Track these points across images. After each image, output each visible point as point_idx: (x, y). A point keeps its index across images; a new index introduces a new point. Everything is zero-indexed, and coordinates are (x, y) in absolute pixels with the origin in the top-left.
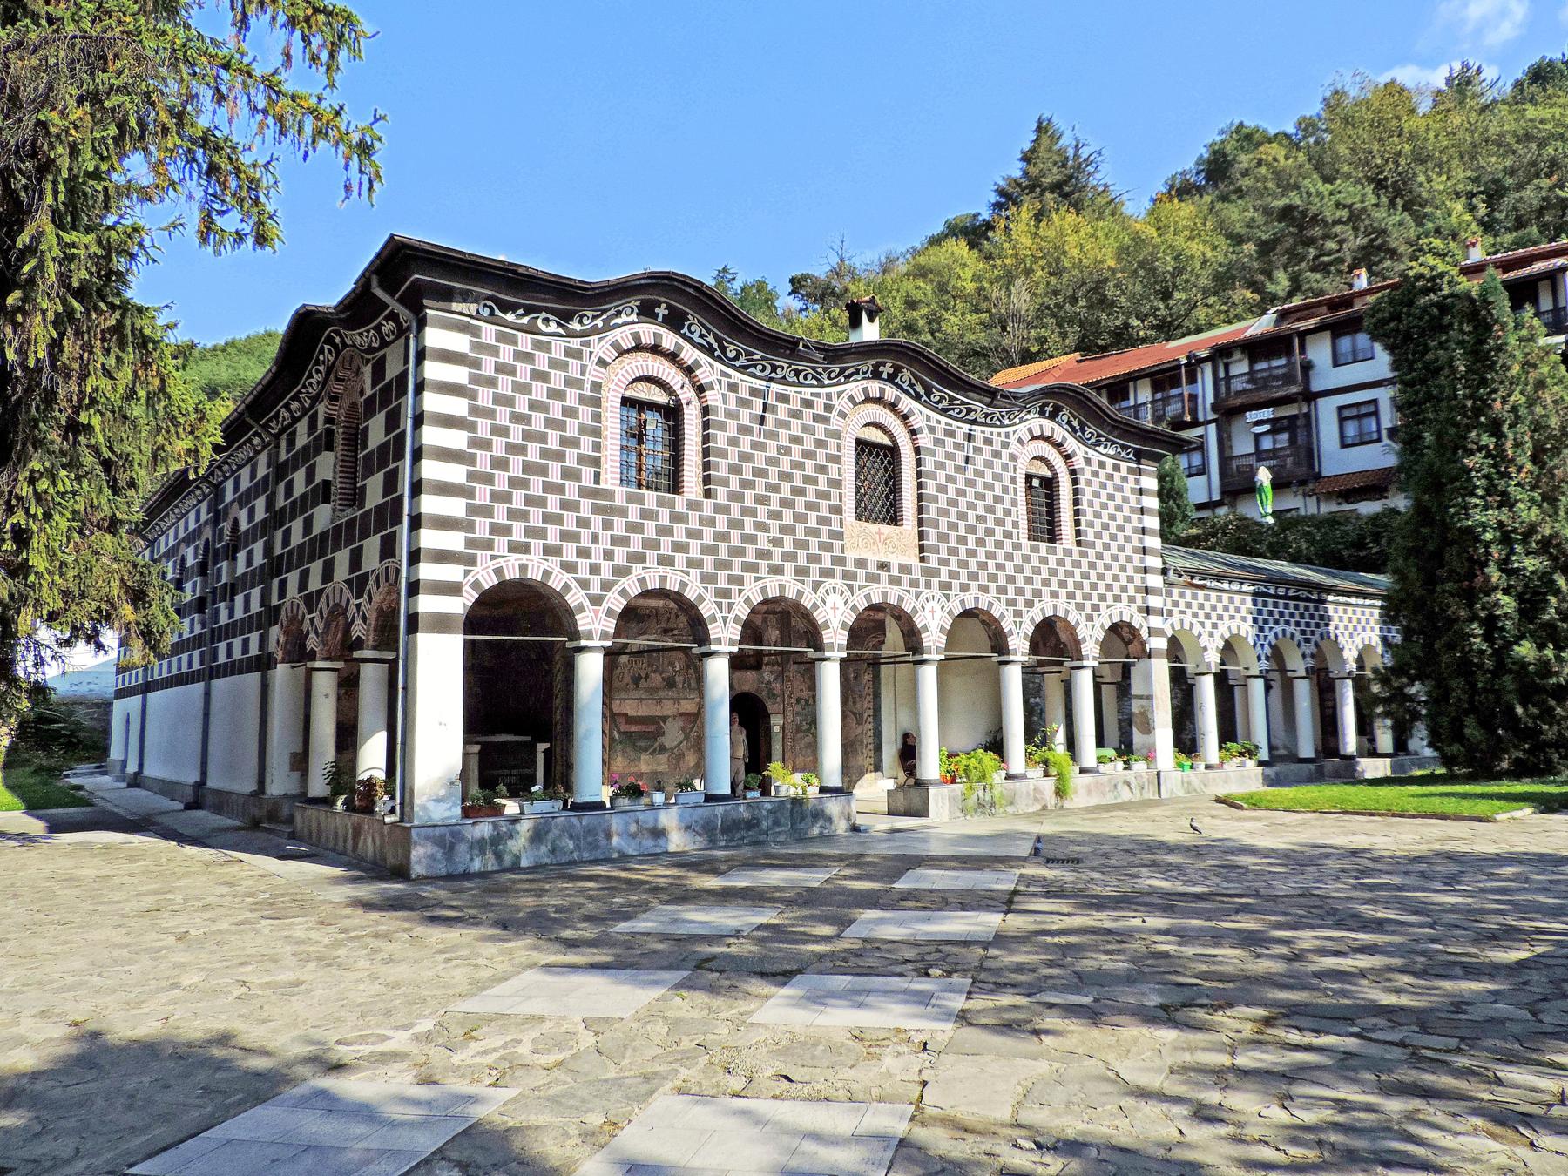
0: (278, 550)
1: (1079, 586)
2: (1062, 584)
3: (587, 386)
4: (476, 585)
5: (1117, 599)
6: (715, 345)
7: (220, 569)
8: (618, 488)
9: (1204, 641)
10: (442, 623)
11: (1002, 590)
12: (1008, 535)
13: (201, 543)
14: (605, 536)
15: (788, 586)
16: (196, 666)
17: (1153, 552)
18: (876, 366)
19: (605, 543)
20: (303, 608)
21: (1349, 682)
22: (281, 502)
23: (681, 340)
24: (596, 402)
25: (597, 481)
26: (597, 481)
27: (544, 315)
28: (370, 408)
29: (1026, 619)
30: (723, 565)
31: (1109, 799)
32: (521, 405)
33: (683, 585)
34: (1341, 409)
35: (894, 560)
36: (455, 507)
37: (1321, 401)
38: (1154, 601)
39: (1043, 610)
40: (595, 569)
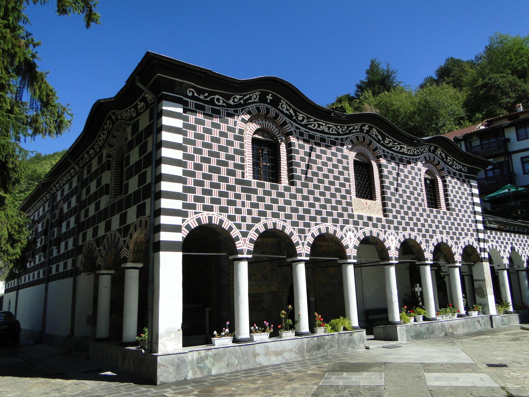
0: (82, 219)
1: (450, 228)
2: (444, 228)
3: (237, 131)
4: (188, 227)
5: (466, 235)
6: (293, 114)
7: (54, 232)
8: (252, 180)
9: (502, 254)
10: (171, 246)
11: (420, 230)
12: (420, 205)
13: (45, 221)
14: (248, 203)
15: (329, 227)
16: (41, 276)
17: (478, 213)
18: (361, 127)
19: (248, 207)
20: (95, 245)
21: (524, 273)
22: (84, 197)
23: (278, 112)
24: (241, 139)
25: (243, 177)
26: (243, 177)
27: (217, 96)
28: (131, 146)
29: (431, 244)
30: (301, 218)
31: (472, 330)
32: (208, 139)
33: (284, 227)
34: (522, 158)
35: (375, 216)
36: (177, 188)
37: (513, 155)
38: (481, 236)
39: (437, 240)
40: (244, 219)
